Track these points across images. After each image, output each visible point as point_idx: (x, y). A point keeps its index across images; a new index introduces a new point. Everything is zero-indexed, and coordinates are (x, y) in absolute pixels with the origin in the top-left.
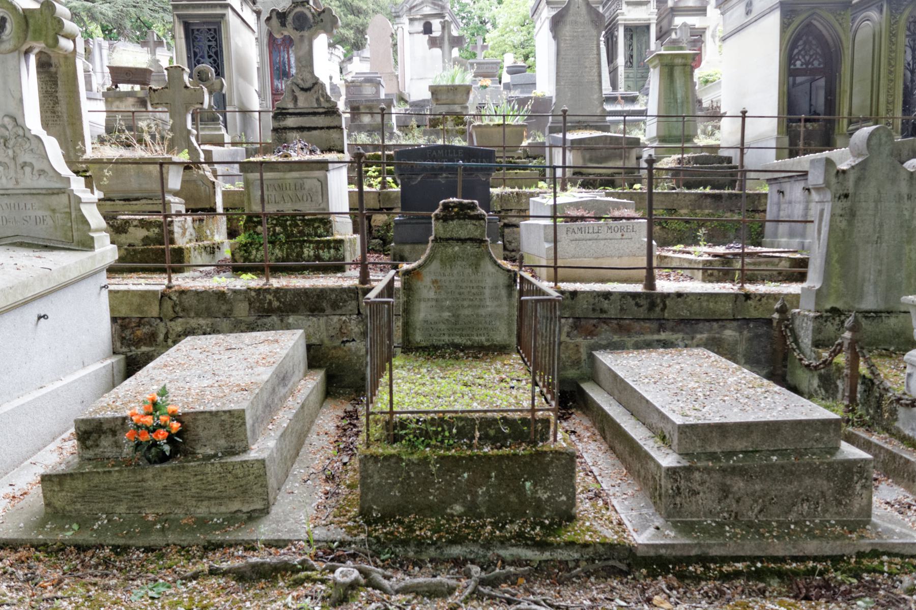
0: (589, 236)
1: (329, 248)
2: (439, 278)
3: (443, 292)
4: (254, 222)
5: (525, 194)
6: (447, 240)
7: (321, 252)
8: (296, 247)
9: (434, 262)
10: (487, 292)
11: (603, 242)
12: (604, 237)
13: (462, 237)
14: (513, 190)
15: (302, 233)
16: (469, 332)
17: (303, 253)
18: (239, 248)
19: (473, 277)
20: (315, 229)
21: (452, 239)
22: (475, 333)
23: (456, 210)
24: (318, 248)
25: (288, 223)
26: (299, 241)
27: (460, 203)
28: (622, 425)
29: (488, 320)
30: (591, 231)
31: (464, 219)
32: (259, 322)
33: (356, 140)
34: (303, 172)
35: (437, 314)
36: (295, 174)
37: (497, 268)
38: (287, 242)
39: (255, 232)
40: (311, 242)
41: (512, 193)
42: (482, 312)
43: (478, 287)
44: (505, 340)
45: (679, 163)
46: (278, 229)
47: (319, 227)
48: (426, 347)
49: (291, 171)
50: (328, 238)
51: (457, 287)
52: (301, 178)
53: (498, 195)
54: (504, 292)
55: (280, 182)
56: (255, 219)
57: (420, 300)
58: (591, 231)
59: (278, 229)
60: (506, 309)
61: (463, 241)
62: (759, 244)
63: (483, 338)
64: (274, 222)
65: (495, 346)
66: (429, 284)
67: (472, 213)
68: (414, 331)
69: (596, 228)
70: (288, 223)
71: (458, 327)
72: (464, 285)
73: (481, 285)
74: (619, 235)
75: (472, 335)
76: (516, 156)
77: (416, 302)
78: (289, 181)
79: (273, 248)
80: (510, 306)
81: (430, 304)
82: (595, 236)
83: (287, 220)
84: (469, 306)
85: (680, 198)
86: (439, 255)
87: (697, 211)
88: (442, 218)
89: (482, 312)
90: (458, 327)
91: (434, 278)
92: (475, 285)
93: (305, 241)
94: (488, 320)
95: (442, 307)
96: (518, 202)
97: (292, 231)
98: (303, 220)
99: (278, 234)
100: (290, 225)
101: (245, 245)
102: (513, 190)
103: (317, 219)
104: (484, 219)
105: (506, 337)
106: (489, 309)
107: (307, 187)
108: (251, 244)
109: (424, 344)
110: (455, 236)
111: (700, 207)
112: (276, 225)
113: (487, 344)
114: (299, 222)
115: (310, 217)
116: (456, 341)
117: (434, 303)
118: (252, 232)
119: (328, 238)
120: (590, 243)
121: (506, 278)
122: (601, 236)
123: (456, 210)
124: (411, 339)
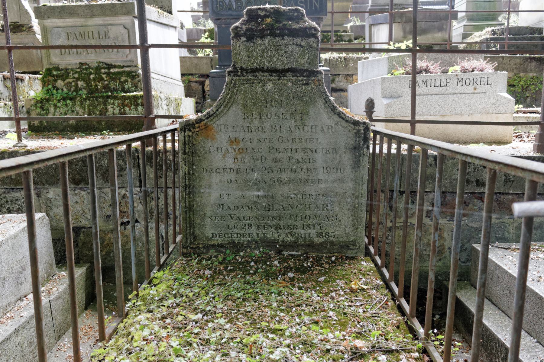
0: (435, 90)
1: (137, 105)
2: (241, 135)
3: (247, 159)
4: (54, 76)
5: (352, 59)
6: (254, 71)
7: (127, 109)
8: (99, 104)
9: (233, 108)
10: (320, 158)
11: (451, 97)
12: (453, 92)
13: (279, 66)
14: (341, 55)
15: (106, 88)
16: (290, 222)
17: (107, 110)
18: (35, 105)
19: (296, 134)
20: (122, 83)
21: (262, 70)
22: (299, 223)
23: (269, 20)
24: (124, 105)
25: (92, 76)
26: (103, 97)
27: (277, 11)
28: (470, 308)
29: (320, 203)
30: (438, 84)
31: (282, 36)
32: (9, 197)
33: (205, 26)
34: (107, 18)
35: (239, 193)
36: (98, 21)
37: (336, 118)
38: (88, 98)
39: (54, 87)
40: (115, 98)
41: (340, 58)
42: (311, 189)
43: (304, 150)
44: (348, 235)
45: (493, 34)
46: (80, 84)
47: (126, 81)
48: (221, 246)
49: (93, 16)
50: (135, 93)
51: (270, 149)
52: (105, 25)
53: (326, 60)
54: (347, 158)
55: (82, 30)
56: (55, 73)
57: (211, 172)
58: (438, 84)
59: (80, 84)
60: (350, 184)
61: (281, 73)
62: (35, 183)
63: (313, 232)
64: (76, 76)
65: (332, 243)
66: (225, 145)
67: (295, 26)
68: (203, 219)
69: (444, 81)
70: (92, 76)
71: (271, 213)
72: (283, 146)
73: (309, 146)
74: (470, 89)
75: (295, 227)
76: (342, 30)
77: (205, 175)
78: (91, 29)
79: (74, 105)
80: (356, 181)
81: (227, 177)
82: (442, 90)
83: (91, 73)
84: (290, 181)
85: (505, 61)
86: (240, 97)
87: (521, 75)
88: (245, 35)
89: (311, 189)
90: (271, 213)
91: (233, 135)
92: (299, 146)
93: (108, 97)
94: (320, 203)
95: (247, 182)
96: (346, 66)
97: (96, 86)
98: (108, 74)
99: (81, 89)
100: (94, 79)
101: (41, 101)
102: (341, 55)
103: (124, 72)
104: (314, 36)
105: (349, 230)
106: (323, 186)
107: (111, 35)
108: (48, 100)
109: (218, 241)
110: (267, 64)
111: (525, 71)
112: (78, 79)
113: (318, 240)
114: (104, 76)
115: (116, 70)
116: (269, 236)
117: (233, 176)
118: (50, 87)
119: (135, 93)
120: (436, 98)
121: (351, 134)
122: (450, 90)
123: (269, 20)
124: (197, 232)
